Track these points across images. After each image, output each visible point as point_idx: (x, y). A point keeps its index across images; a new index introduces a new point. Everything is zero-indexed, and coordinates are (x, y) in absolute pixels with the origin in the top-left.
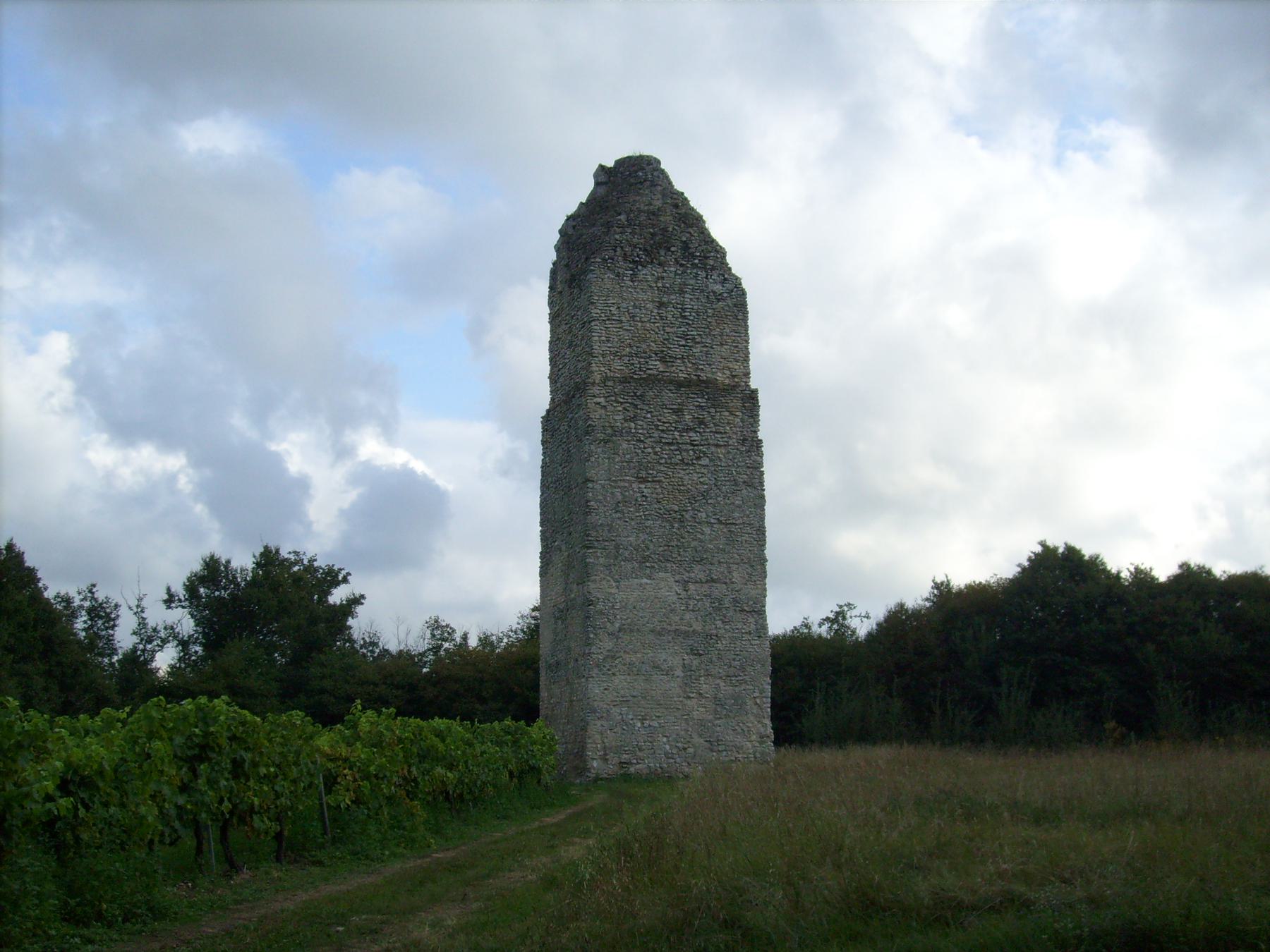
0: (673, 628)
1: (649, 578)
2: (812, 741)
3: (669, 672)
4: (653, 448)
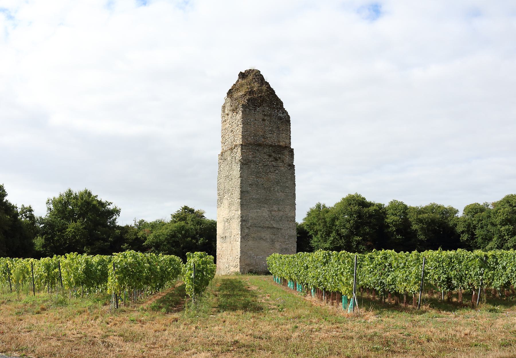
1: (260, 209)
2: (377, 205)
3: (265, 240)
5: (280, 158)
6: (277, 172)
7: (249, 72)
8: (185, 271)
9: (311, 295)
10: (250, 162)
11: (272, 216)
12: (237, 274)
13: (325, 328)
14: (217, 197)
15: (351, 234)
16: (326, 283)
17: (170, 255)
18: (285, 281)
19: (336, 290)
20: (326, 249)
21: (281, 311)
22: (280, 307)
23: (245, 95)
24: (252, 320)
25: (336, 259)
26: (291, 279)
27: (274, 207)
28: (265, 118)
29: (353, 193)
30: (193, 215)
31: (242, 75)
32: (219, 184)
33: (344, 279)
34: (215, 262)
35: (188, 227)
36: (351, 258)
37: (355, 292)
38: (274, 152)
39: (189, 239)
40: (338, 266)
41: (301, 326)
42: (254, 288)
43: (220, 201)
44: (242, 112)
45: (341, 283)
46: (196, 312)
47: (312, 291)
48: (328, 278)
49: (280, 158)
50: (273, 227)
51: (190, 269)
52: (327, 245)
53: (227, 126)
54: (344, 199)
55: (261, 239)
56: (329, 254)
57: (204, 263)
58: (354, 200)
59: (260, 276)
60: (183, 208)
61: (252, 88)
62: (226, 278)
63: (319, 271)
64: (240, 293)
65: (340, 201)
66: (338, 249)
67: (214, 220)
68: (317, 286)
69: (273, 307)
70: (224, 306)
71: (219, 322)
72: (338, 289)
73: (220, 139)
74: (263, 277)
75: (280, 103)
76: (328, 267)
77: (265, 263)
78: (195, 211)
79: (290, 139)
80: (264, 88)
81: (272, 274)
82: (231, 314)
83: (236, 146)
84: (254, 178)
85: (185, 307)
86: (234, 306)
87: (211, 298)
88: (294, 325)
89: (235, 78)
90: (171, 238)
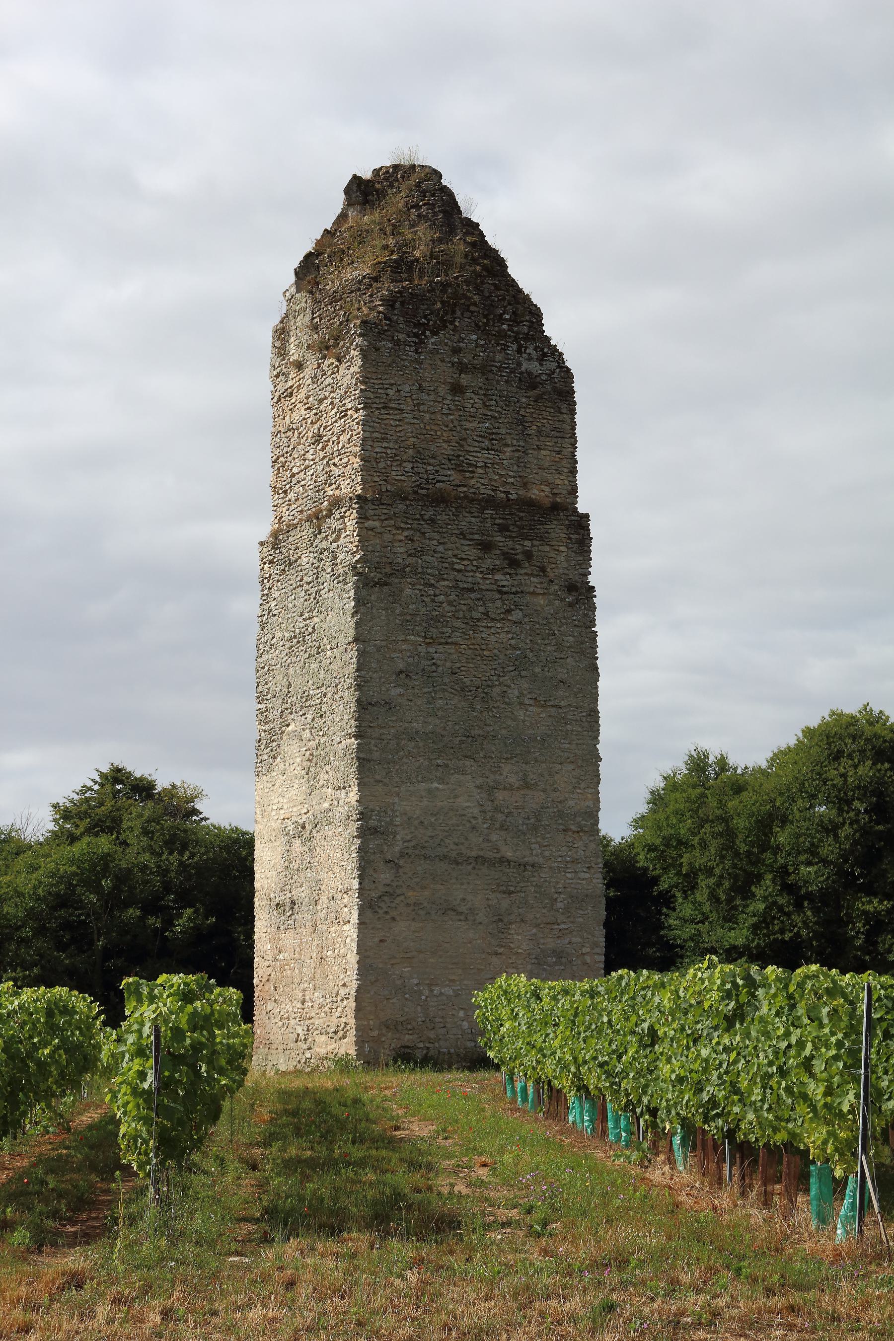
0: (474, 854)
1: (441, 780)
4: (446, 595)
5: (529, 555)
6: (516, 615)
7: (393, 176)
8: (117, 1058)
9: (671, 1161)
10: (401, 572)
11: (497, 809)
12: (343, 1065)
13: (734, 1312)
14: (254, 730)
15: (847, 883)
16: (736, 1109)
17: (50, 985)
18: (556, 1095)
19: (781, 1137)
20: (731, 955)
21: (539, 1235)
22: (537, 1215)
23: (376, 279)
24: (413, 1278)
25: (781, 1000)
26: (582, 1088)
27: (506, 768)
28: (465, 379)
29: (851, 708)
30: (147, 809)
31: (362, 192)
32: (264, 671)
33: (816, 1090)
34: (248, 1014)
35: (128, 859)
36: (844, 995)
37: (865, 1150)
38: (503, 529)
39: (133, 912)
40: (787, 1034)
41: (631, 1302)
42: (419, 1129)
43: (269, 744)
44: (364, 355)
45: (802, 1109)
46: (164, 1242)
47: (677, 1140)
48: (744, 1085)
49: (529, 555)
50: (504, 861)
51: (140, 1052)
52: (738, 936)
53: (296, 416)
54: (809, 732)
55: (449, 910)
56: (748, 978)
57: (200, 1022)
58: (854, 738)
59: (448, 1076)
60: (102, 775)
61: (404, 247)
62: (297, 1084)
63: (704, 1053)
64: (357, 1153)
65: (793, 742)
66: (789, 957)
67: (244, 827)
68: (699, 1120)
69: (504, 1214)
70: (288, 1214)
71: (267, 1288)
72: (793, 1135)
73: (268, 475)
74: (457, 1078)
75: (527, 315)
76: (747, 1035)
77: (468, 1017)
78: (158, 789)
79: (573, 471)
80: (459, 246)
81: (497, 1068)
82: (320, 1247)
83: (336, 503)
84: (416, 644)
85: (115, 1221)
86: (331, 1213)
87: (229, 1178)
88: (597, 1298)
89: (335, 202)
90: (54, 908)
